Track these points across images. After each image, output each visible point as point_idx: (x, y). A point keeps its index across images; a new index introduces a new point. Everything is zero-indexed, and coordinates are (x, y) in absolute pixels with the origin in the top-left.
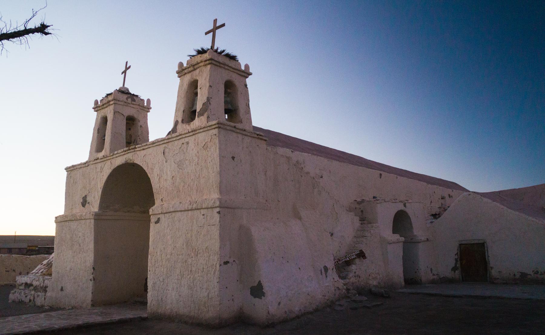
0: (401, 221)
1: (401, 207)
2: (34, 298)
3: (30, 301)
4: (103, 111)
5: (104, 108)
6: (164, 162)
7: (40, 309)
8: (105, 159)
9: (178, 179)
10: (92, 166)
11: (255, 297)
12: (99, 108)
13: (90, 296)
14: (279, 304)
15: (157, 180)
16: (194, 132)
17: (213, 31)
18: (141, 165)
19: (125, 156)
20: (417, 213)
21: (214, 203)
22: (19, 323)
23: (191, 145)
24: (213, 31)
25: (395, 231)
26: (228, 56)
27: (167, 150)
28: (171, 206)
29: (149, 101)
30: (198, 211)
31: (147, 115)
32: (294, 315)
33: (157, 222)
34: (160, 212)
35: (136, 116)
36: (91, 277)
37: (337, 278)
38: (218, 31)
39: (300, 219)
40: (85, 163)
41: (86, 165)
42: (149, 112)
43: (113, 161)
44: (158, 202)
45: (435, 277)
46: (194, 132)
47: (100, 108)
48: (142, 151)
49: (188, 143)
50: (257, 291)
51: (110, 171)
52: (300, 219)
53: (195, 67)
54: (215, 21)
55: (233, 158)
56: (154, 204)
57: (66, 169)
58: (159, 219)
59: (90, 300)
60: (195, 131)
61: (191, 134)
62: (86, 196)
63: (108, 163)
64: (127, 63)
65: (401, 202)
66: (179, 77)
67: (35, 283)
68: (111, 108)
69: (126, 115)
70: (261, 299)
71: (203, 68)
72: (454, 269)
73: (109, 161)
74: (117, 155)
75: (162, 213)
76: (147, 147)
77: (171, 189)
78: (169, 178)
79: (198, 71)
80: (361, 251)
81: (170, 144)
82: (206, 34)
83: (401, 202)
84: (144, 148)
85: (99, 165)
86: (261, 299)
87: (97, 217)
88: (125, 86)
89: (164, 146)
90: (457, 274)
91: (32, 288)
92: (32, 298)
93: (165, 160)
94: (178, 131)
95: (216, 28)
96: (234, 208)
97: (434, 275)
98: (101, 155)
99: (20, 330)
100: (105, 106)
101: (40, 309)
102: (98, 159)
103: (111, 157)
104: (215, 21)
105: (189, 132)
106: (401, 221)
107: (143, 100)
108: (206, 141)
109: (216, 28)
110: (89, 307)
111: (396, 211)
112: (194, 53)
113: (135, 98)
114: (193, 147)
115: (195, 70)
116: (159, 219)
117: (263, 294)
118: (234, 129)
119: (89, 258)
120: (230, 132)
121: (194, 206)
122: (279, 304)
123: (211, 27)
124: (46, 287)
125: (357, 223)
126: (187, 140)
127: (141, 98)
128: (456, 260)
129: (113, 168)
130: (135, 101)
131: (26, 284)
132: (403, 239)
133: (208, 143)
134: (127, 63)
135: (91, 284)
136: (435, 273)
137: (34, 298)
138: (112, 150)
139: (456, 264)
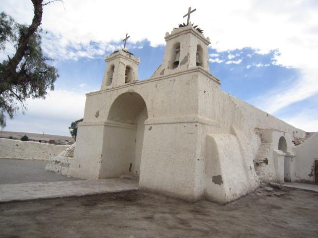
0: (282, 143)
1: (282, 135)
2: (61, 170)
3: (58, 171)
7: (65, 178)
10: (104, 94)
11: (216, 183)
13: (98, 173)
14: (230, 189)
16: (180, 73)
17: (188, 15)
19: (127, 88)
20: (289, 139)
22: (57, 187)
24: (188, 15)
25: (280, 149)
26: (198, 30)
27: (158, 84)
30: (181, 124)
32: (236, 198)
33: (150, 129)
34: (152, 123)
36: (100, 160)
37: (256, 175)
38: (191, 14)
39: (235, 135)
40: (100, 92)
43: (119, 91)
45: (298, 179)
46: (180, 73)
49: (174, 80)
50: (218, 180)
52: (235, 135)
54: (190, 8)
55: (205, 92)
56: (147, 117)
57: (86, 95)
58: (151, 128)
59: (98, 174)
60: (181, 72)
61: (178, 75)
62: (99, 111)
63: (116, 91)
64: (127, 34)
65: (282, 132)
66: (166, 41)
67: (62, 161)
69: (126, 65)
70: (220, 185)
72: (311, 175)
75: (154, 124)
79: (180, 37)
80: (266, 159)
82: (184, 17)
83: (282, 132)
85: (109, 93)
86: (220, 185)
87: (107, 125)
90: (312, 179)
91: (60, 164)
92: (60, 170)
95: (190, 12)
96: (204, 124)
97: (296, 177)
98: (110, 87)
99: (60, 194)
101: (65, 178)
104: (190, 8)
105: (176, 74)
106: (282, 143)
109: (190, 12)
110: (97, 179)
111: (280, 137)
112: (178, 27)
116: (151, 128)
117: (222, 182)
118: (206, 74)
119: (100, 149)
120: (203, 75)
121: (178, 121)
122: (230, 189)
123: (187, 12)
124: (69, 164)
125: (260, 142)
126: (173, 78)
128: (312, 170)
130: (131, 57)
131: (56, 161)
132: (285, 154)
134: (127, 34)
135: (99, 165)
136: (297, 176)
137: (61, 170)
139: (312, 172)
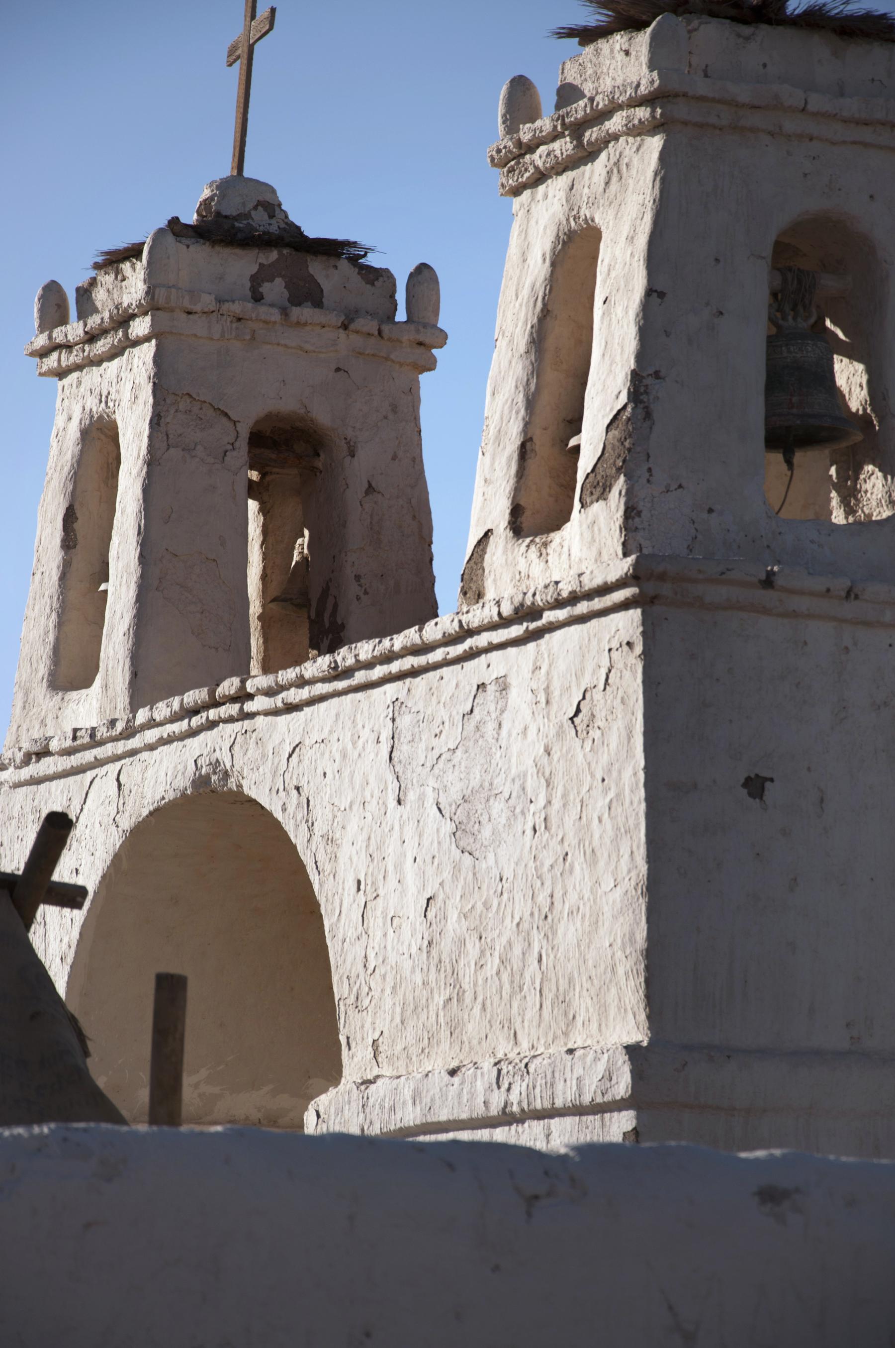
4: (92, 377)
5: (97, 362)
6: (392, 803)
8: (88, 756)
9: (453, 916)
12: (67, 359)
15: (356, 916)
18: (278, 815)
19: (195, 745)
21: (609, 1076)
23: (518, 696)
28: (407, 1094)
29: (423, 276)
31: (412, 393)
35: (322, 415)
41: (869, 371)
42: (430, 365)
43: (132, 769)
44: (355, 1063)
47: (74, 358)
48: (282, 720)
49: (503, 685)
51: (115, 840)
53: (591, 135)
61: (516, 631)
68: (143, 358)
71: (626, 146)
73: (112, 769)
74: (151, 736)
76: (304, 693)
77: (418, 978)
78: (413, 908)
79: (598, 168)
81: (420, 683)
84: (294, 695)
88: (246, 174)
89: (390, 689)
93: (393, 786)
94: (490, 594)
98: (87, 708)
100: (101, 346)
102: (44, 753)
103: (121, 747)
107: (380, 278)
108: (586, 682)
113: (316, 268)
114: (526, 712)
115: (586, 155)
127: (373, 260)
129: (126, 823)
133: (597, 695)
138: (141, 691)
